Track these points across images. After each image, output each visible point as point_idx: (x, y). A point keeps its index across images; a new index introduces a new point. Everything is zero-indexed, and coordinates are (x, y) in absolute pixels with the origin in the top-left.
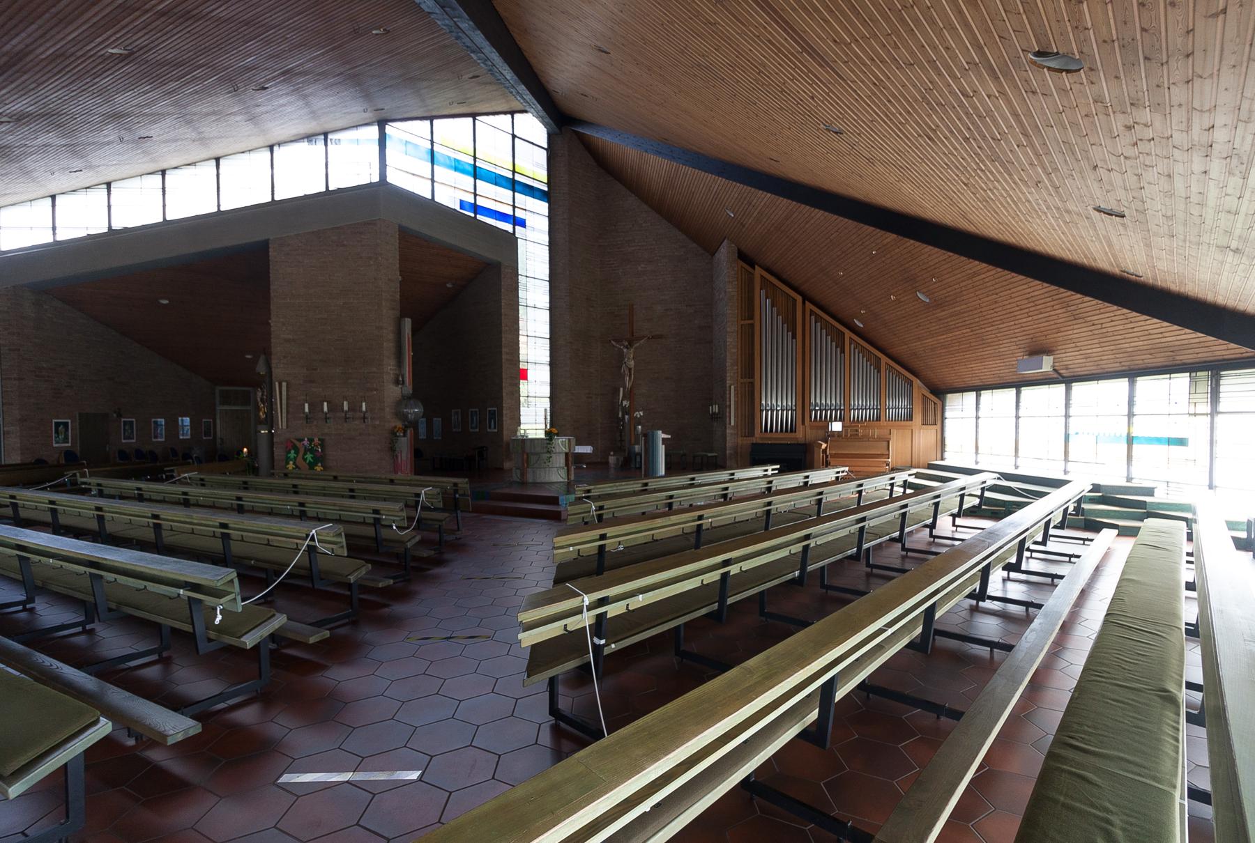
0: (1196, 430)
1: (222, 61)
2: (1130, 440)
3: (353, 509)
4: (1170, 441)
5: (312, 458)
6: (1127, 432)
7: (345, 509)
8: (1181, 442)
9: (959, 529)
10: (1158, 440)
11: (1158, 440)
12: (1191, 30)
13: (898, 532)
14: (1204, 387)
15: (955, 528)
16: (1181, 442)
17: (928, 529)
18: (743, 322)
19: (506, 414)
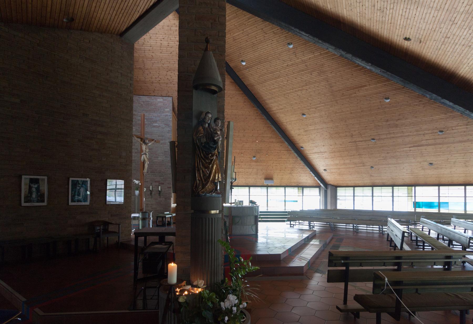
0: (299, 199)
1: (217, 229)
2: (285, 201)
3: (427, 257)
4: (294, 201)
5: (134, 182)
6: (284, 199)
7: (431, 257)
8: (297, 201)
9: (454, 246)
10: (292, 201)
11: (292, 201)
12: (447, 38)
13: (311, 243)
14: (301, 191)
15: (412, 241)
16: (297, 201)
17: (415, 239)
18: (158, 310)
19: (171, 118)
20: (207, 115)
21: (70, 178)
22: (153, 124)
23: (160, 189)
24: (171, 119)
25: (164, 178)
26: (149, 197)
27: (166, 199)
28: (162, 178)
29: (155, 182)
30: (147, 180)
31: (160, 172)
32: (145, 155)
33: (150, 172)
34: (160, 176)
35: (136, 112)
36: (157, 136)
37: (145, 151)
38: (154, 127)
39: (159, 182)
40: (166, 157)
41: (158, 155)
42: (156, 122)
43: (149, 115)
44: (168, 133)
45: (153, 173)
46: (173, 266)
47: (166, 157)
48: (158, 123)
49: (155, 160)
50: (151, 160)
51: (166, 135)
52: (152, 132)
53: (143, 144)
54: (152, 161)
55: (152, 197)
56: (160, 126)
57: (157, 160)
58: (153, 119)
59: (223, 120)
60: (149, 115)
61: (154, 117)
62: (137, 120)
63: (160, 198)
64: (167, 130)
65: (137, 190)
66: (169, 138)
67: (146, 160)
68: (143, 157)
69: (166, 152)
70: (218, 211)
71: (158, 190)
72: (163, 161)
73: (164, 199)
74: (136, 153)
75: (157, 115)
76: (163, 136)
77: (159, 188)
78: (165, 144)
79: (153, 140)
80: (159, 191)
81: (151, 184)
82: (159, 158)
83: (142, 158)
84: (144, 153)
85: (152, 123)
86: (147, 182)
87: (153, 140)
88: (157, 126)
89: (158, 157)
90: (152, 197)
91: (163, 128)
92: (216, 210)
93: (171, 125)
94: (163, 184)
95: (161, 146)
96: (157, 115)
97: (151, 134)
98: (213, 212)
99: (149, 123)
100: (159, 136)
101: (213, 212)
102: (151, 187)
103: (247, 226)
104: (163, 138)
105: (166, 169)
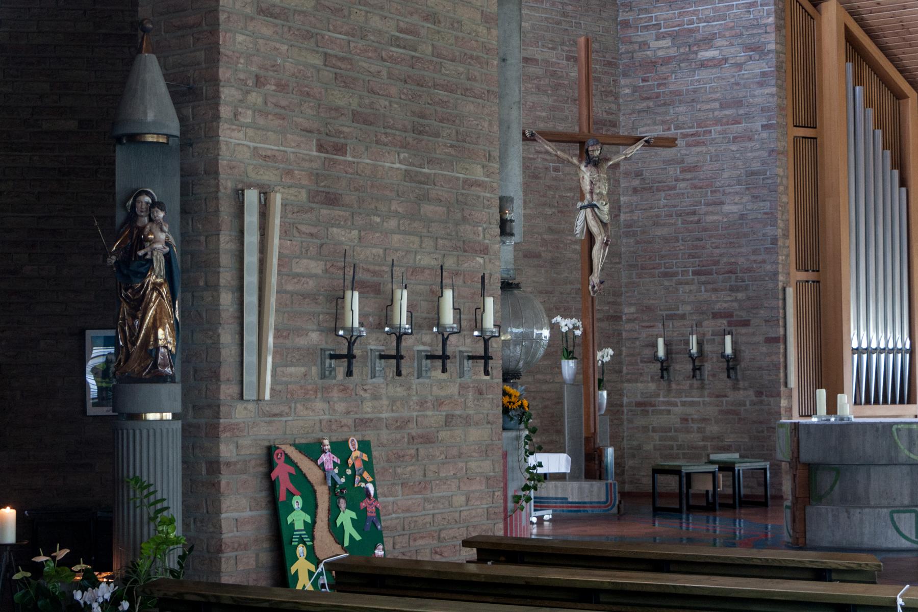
20: (137, 199)
21: (88, 332)
22: (696, 53)
23: (729, 350)
24: (771, 20)
25: (749, 298)
26: (691, 386)
27: (759, 394)
28: (740, 295)
29: (716, 316)
30: (680, 312)
31: (731, 272)
32: (589, 210)
33: (694, 273)
34: (732, 289)
35: (631, 10)
36: (716, 105)
37: (591, 192)
38: (704, 65)
39: (727, 315)
40: (755, 198)
41: (724, 194)
42: (708, 41)
43: (680, 14)
44: (761, 84)
45: (703, 278)
46: (26, 512)
47: (755, 198)
48: (717, 48)
49: (710, 218)
50: (696, 218)
51: (754, 96)
52: (695, 91)
53: (583, 168)
54: (698, 222)
55: (702, 387)
56: (726, 60)
57: (715, 218)
58: (698, 29)
59: (217, 192)
60: (680, 14)
61: (700, 20)
62: (636, 47)
63: (735, 388)
64: (757, 71)
65: (568, 358)
66: (763, 110)
67: (595, 229)
68: (583, 219)
69: (753, 173)
70: (168, 416)
71: (723, 355)
72: (742, 217)
73: (751, 393)
74: (635, 191)
75: (715, 10)
76: (738, 103)
77: (655, 345)
78: (750, 139)
79: (639, 139)
80: (727, 359)
81: (699, 324)
82: (727, 208)
83: (580, 223)
84: (586, 203)
85: (695, 48)
86: (683, 317)
87: (639, 139)
88: (713, 58)
89: (722, 203)
90: (702, 387)
91: (739, 66)
92: (161, 412)
93: (772, 46)
94: (746, 323)
95: (734, 148)
96: (715, 10)
97: (693, 101)
98: (151, 416)
99: (682, 50)
100: (722, 107)
101: (151, 416)
102: (694, 340)
103: (867, 510)
104: (741, 112)
105: (754, 252)
